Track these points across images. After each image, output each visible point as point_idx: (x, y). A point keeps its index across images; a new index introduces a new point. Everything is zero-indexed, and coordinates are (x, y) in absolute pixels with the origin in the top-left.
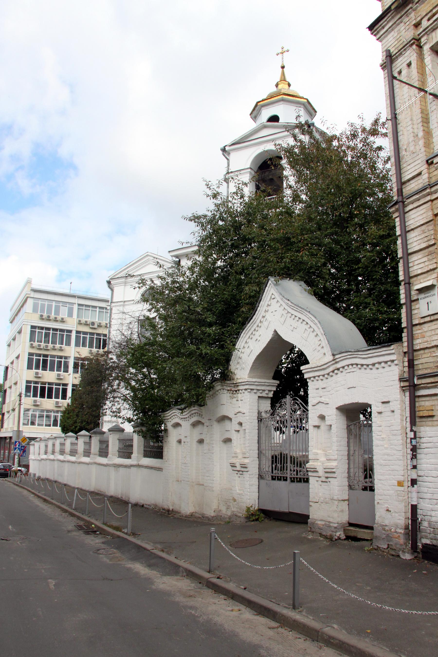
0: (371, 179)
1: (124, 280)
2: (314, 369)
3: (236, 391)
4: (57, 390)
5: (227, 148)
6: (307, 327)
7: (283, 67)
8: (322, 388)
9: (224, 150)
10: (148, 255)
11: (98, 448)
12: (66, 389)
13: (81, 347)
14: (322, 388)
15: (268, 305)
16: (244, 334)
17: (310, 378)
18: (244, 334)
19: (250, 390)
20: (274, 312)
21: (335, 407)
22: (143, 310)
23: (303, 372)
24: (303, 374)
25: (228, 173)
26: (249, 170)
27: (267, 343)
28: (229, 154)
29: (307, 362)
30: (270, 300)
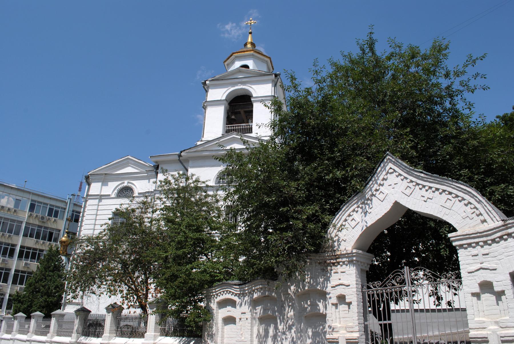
0: (510, 136)
3: (334, 264)
4: (12, 226)
6: (445, 196)
8: (483, 255)
12: (9, 273)
13: (18, 285)
14: (483, 255)
15: (384, 179)
16: (343, 211)
17: (461, 246)
18: (340, 215)
20: (393, 185)
21: (508, 272)
23: (451, 239)
27: (383, 214)
28: (208, 87)
29: (455, 230)
30: (386, 174)
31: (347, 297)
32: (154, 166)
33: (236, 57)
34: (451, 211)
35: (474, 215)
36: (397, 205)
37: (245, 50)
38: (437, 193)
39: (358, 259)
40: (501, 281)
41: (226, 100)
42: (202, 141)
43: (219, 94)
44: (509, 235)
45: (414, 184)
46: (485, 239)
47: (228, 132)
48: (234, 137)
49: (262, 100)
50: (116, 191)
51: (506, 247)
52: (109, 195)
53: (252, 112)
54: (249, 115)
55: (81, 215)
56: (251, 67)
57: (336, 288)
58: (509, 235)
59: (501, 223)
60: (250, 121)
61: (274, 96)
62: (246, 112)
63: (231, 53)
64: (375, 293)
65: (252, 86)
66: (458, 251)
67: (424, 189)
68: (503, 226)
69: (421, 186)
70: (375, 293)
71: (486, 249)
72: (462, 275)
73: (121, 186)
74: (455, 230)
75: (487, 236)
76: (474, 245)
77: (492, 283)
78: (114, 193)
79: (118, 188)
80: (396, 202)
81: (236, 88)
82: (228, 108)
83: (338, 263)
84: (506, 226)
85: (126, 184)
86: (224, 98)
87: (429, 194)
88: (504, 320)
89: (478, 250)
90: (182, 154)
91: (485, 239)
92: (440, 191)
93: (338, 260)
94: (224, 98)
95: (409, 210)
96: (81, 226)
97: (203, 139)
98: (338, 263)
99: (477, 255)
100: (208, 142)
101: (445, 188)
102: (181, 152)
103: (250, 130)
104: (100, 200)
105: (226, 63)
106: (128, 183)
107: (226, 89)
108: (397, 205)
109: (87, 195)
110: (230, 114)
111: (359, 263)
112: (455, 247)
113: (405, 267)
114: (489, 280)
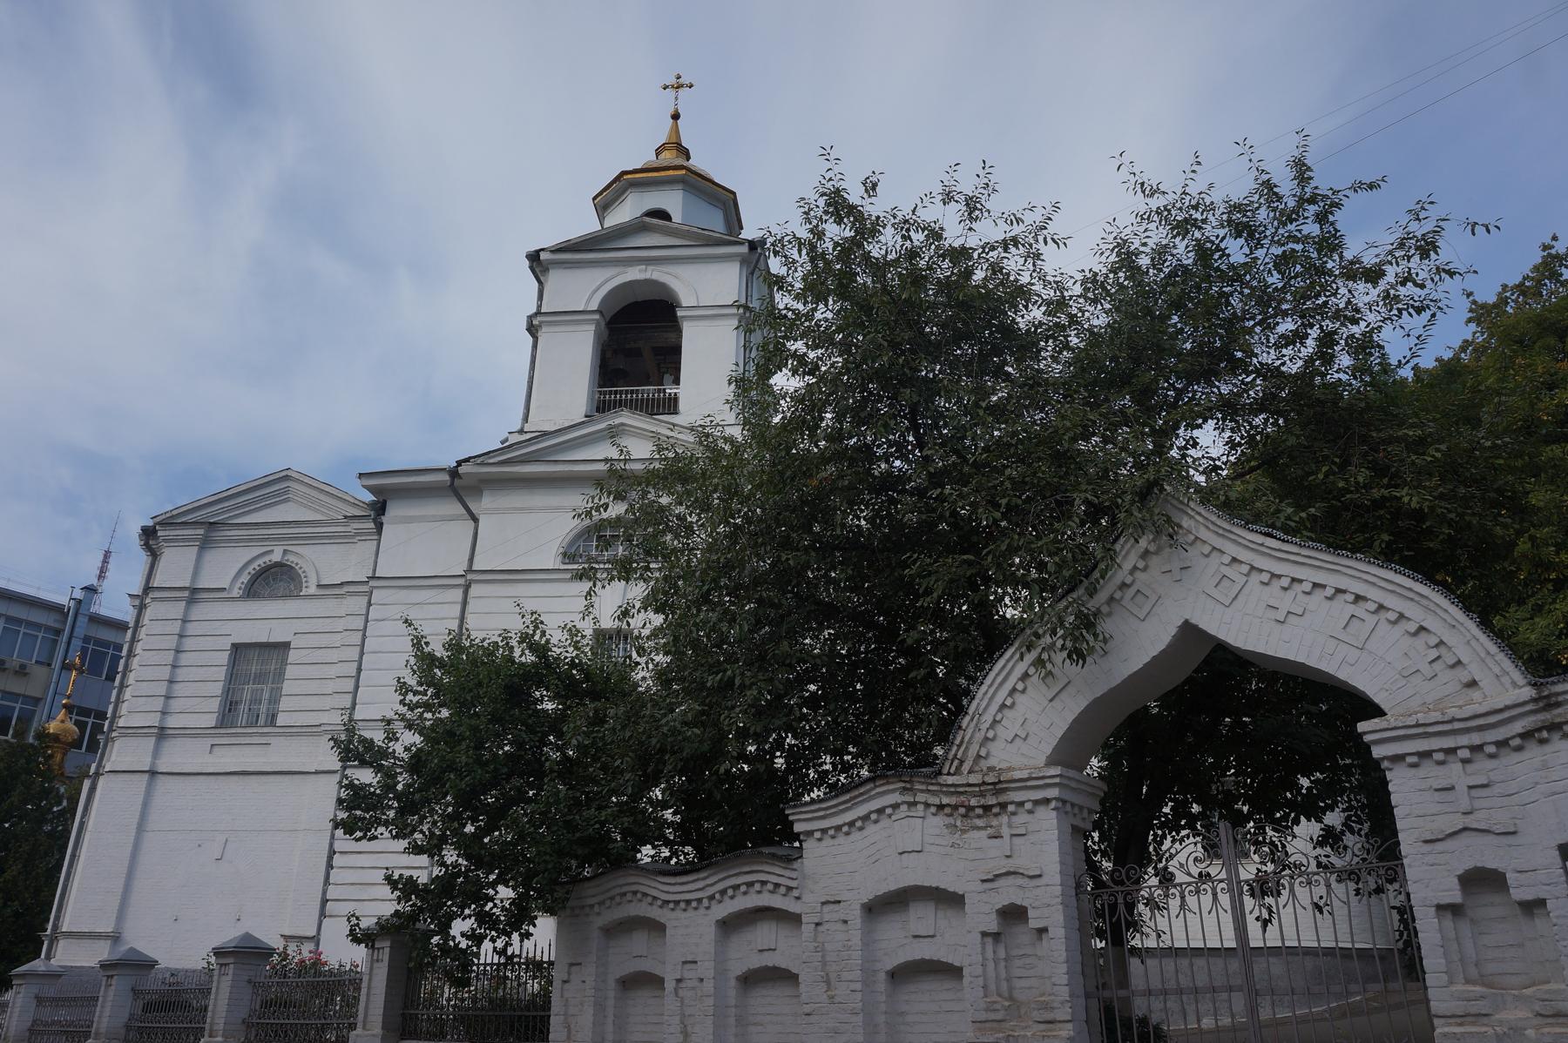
1: (201, 532)
2: (1481, 721)
5: (543, 256)
6: (1342, 607)
7: (676, 117)
9: (534, 257)
10: (287, 478)
11: (127, 1015)
19: (1414, 759)
21: (1555, 843)
22: (1469, 332)
24: (792, 823)
25: (538, 313)
26: (597, 317)
28: (546, 270)
31: (1031, 913)
32: (372, 505)
35: (1438, 666)
36: (1189, 631)
38: (1319, 595)
39: (1068, 796)
40: (1531, 866)
41: (599, 311)
44: (1553, 727)
45: (1245, 569)
46: (1476, 739)
47: (602, 407)
49: (713, 313)
50: (245, 578)
51: (1545, 766)
54: (669, 361)
55: (124, 653)
56: (677, 217)
58: (1553, 727)
59: (1528, 693)
60: (668, 378)
61: (746, 308)
62: (658, 351)
64: (1120, 900)
66: (1389, 775)
67: (1276, 584)
68: (1534, 700)
69: (1265, 577)
70: (1120, 900)
71: (1483, 769)
72: (1404, 849)
73: (260, 562)
74: (1378, 712)
75: (1480, 728)
76: (1491, 749)
77: (1504, 874)
78: (238, 585)
79: (250, 569)
80: (1186, 622)
83: (1003, 806)
84: (1548, 703)
85: (276, 557)
86: (594, 306)
87: (1286, 602)
88: (1548, 992)
89: (1454, 773)
91: (1474, 740)
92: (1329, 592)
93: (1003, 798)
95: (1221, 647)
96: (122, 686)
98: (1003, 806)
99: (1452, 788)
101: (1343, 583)
103: (671, 405)
104: (191, 601)
106: (285, 552)
108: (1189, 631)
110: (609, 355)
111: (1068, 807)
112: (1377, 762)
113: (1221, 825)
114: (1491, 864)
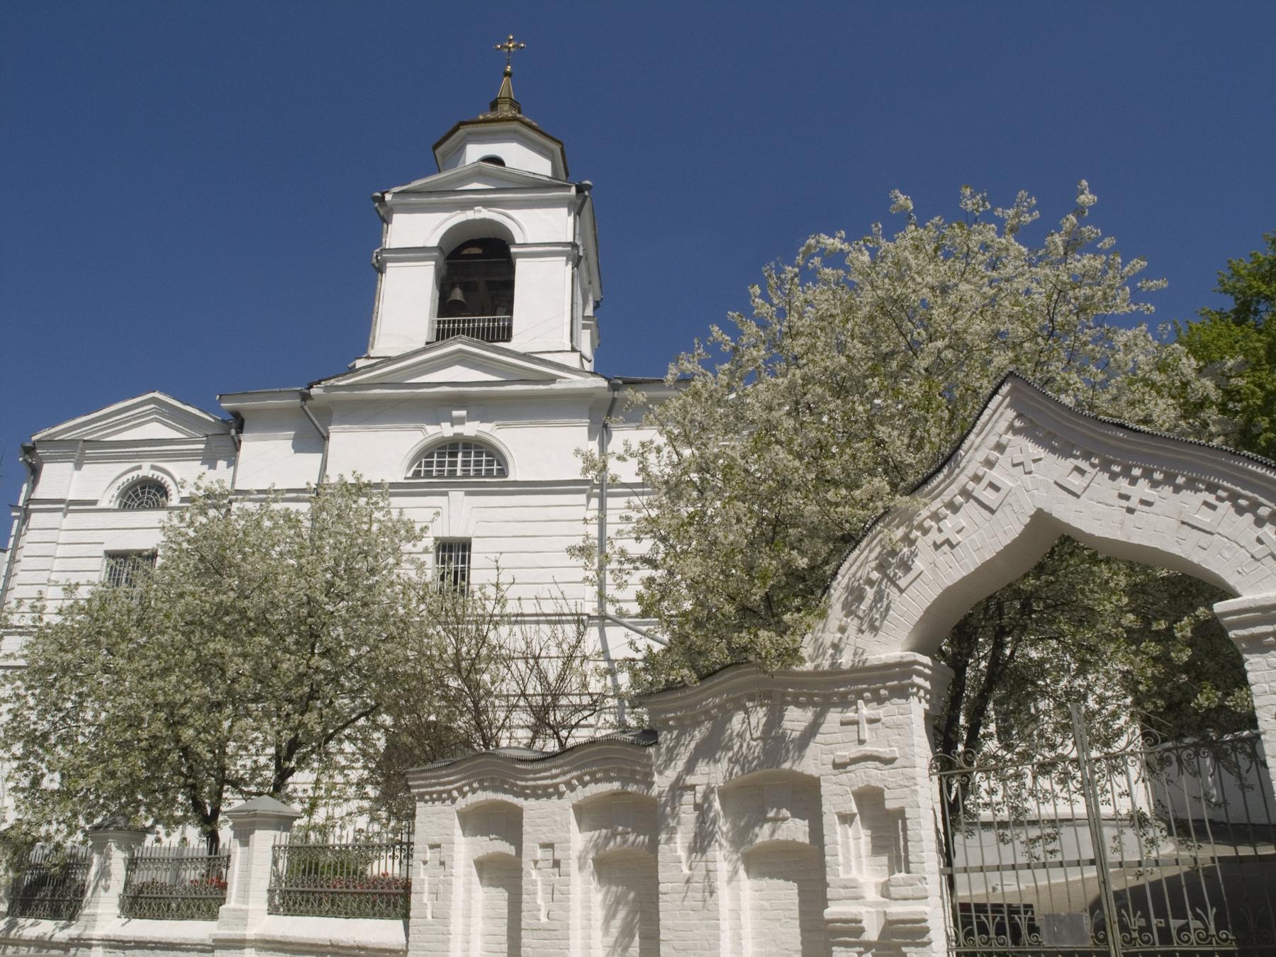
28: (391, 211)
29: (1233, 594)
31: (887, 794)
33: (468, 134)
34: (1216, 537)
37: (490, 116)
41: (439, 248)
42: (368, 358)
43: (417, 229)
47: (442, 335)
48: (460, 351)
52: (94, 502)
53: (509, 285)
57: (849, 768)
63: (455, 124)
65: (511, 212)
81: (470, 215)
82: (444, 272)
85: (146, 471)
90: (315, 391)
94: (434, 241)
97: (372, 353)
100: (388, 360)
102: (311, 387)
103: (506, 334)
105: (439, 151)
107: (446, 215)
108: (1041, 519)
109: (29, 501)
